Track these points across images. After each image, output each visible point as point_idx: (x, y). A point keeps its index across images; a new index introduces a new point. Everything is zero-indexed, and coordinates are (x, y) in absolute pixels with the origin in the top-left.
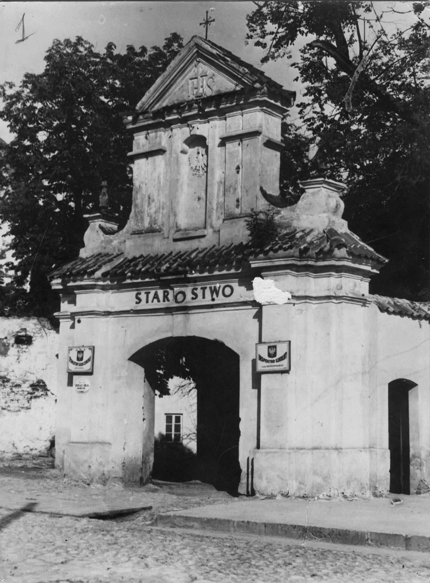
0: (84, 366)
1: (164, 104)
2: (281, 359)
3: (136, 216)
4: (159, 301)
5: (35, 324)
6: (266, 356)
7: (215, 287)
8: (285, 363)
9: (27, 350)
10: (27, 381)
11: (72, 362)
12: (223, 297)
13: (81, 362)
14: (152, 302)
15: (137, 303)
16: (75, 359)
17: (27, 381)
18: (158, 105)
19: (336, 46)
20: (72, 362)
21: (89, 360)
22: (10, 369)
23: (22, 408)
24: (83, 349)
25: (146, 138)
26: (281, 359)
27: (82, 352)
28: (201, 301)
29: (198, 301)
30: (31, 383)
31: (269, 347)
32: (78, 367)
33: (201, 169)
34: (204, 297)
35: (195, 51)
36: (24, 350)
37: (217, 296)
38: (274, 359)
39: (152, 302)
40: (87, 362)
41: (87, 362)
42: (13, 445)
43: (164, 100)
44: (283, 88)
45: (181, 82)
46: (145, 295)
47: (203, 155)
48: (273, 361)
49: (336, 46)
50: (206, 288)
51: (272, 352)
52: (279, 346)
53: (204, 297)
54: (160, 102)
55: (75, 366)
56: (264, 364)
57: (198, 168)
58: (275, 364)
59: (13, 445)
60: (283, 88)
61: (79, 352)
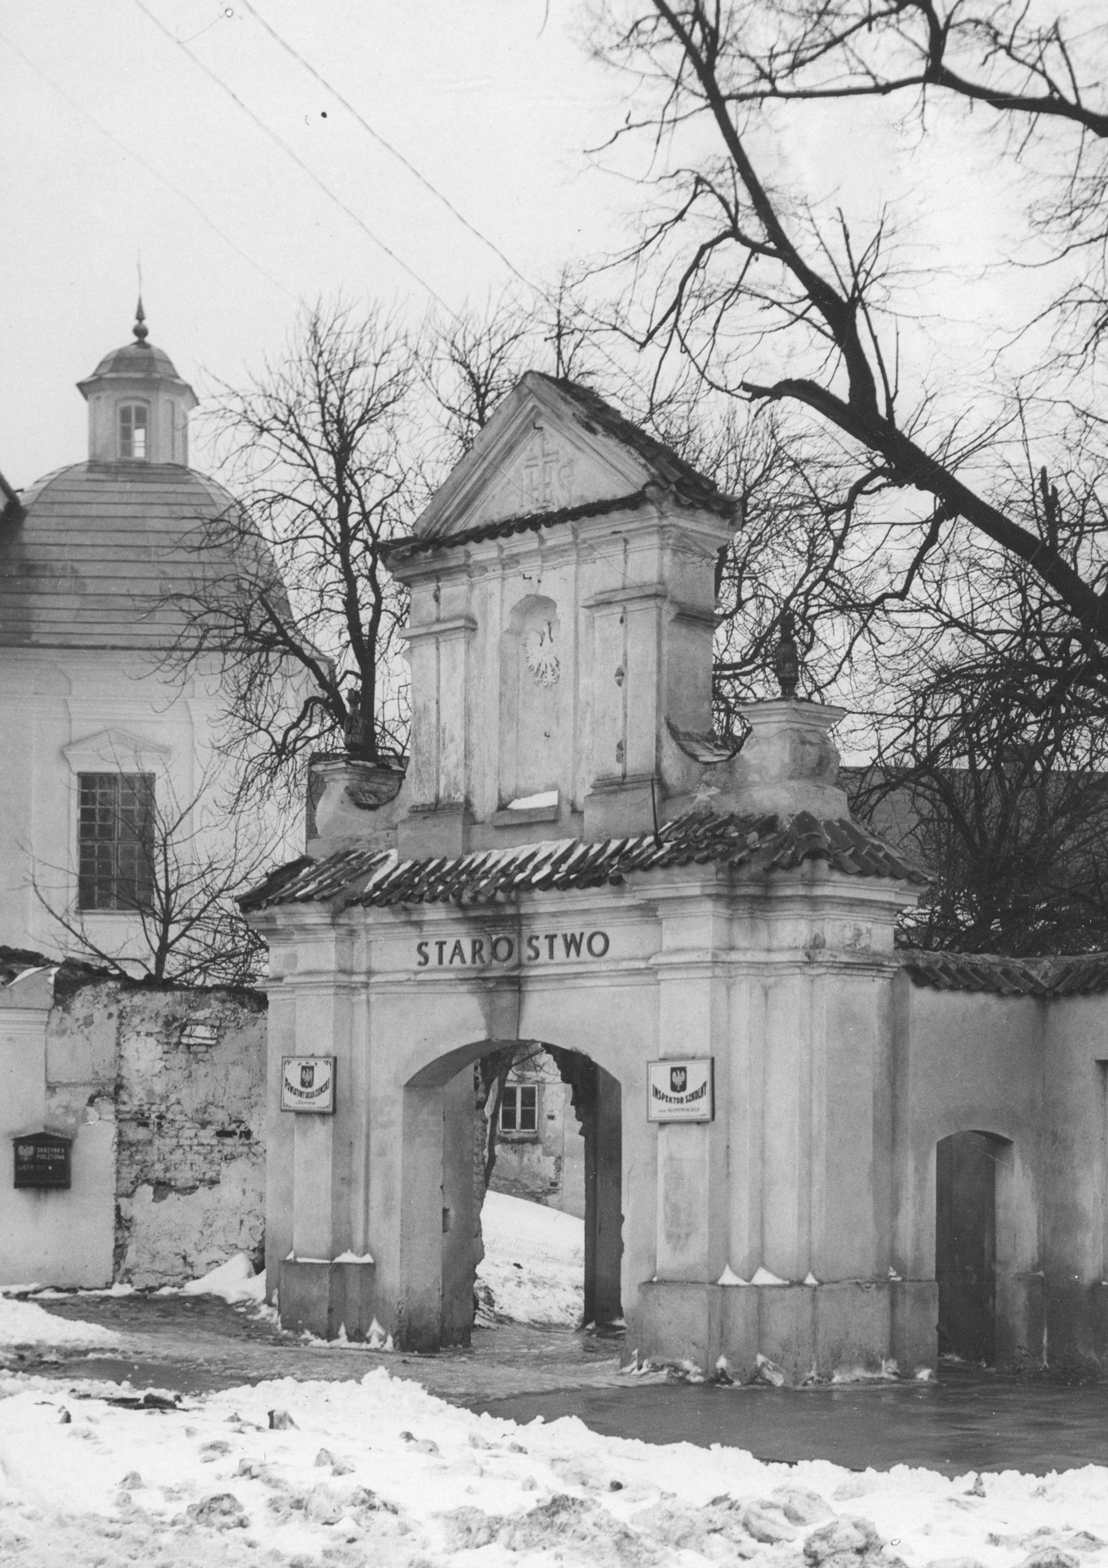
0: (314, 1099)
1: (472, 524)
2: (695, 1096)
3: (418, 771)
4: (463, 961)
5: (223, 1001)
6: (666, 1089)
7: (573, 935)
8: (702, 1106)
9: (207, 1056)
10: (210, 1123)
11: (291, 1089)
12: (590, 958)
13: (309, 1090)
14: (451, 962)
15: (420, 964)
16: (296, 1084)
17: (210, 1123)
18: (461, 522)
19: (846, 400)
20: (291, 1089)
21: (326, 1085)
22: (173, 1098)
23: (201, 1181)
24: (312, 1063)
25: (437, 598)
26: (695, 1096)
27: (312, 1068)
28: (545, 965)
29: (539, 966)
30: (219, 1128)
31: (673, 1070)
32: (304, 1099)
33: (549, 669)
34: (551, 956)
35: (530, 405)
36: (200, 1056)
37: (578, 953)
38: (683, 1094)
39: (451, 962)
40: (321, 1090)
41: (321, 1090)
42: (184, 1258)
43: (472, 515)
44: (540, 1418)
45: (511, 470)
46: (437, 948)
47: (283, 1449)
48: (680, 1101)
49: (846, 400)
50: (555, 936)
51: (678, 1080)
52: (691, 1067)
53: (551, 956)
54: (464, 518)
55: (297, 1098)
56: (663, 1104)
57: (543, 668)
58: (685, 1105)
59: (184, 1258)
60: (540, 1418)
61: (304, 1068)
